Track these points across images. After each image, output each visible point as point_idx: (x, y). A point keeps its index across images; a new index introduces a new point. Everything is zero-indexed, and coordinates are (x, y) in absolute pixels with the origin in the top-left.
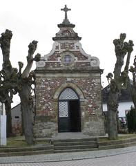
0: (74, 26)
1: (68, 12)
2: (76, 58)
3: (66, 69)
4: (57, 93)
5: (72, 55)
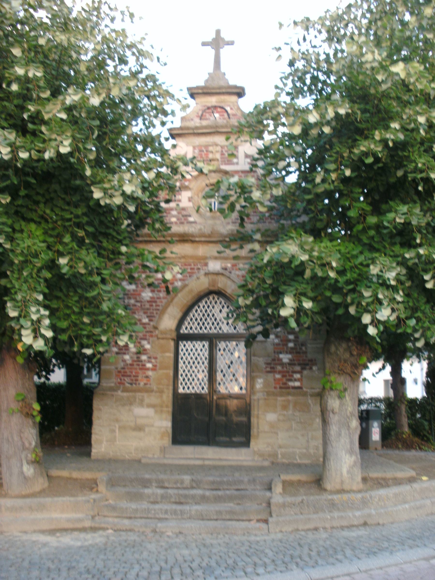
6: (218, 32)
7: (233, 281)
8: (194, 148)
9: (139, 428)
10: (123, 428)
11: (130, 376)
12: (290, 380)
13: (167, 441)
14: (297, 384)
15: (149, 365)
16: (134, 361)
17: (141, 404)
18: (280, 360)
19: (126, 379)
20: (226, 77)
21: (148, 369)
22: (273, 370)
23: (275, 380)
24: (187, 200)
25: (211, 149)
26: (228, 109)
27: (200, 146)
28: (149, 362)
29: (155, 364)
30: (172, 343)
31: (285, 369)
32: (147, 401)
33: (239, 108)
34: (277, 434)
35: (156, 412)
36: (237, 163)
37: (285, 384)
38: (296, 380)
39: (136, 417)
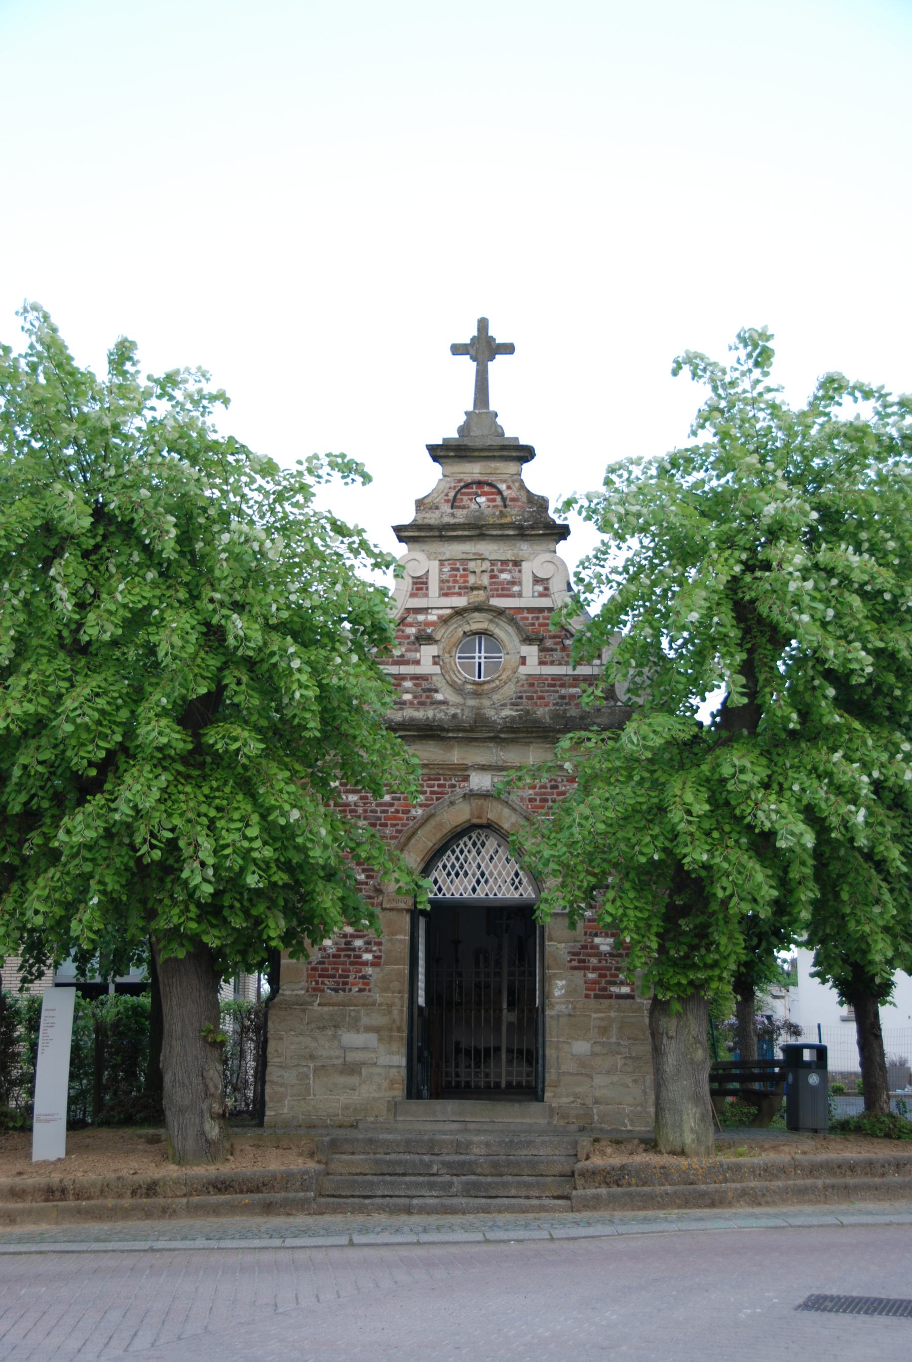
0: (525, 454)
1: (498, 366)
2: (531, 652)
3: (466, 716)
4: (413, 859)
5: (504, 632)
6: (483, 324)
7: (514, 810)
8: (442, 563)
9: (351, 1069)
10: (321, 1070)
11: (333, 976)
12: (614, 983)
13: (399, 1091)
14: (625, 990)
15: (368, 957)
16: (339, 950)
17: (355, 1026)
18: (596, 947)
19: (326, 980)
20: (499, 421)
21: (365, 964)
22: (582, 966)
23: (586, 982)
24: (430, 660)
25: (472, 565)
26: (503, 487)
27: (453, 561)
28: (367, 951)
29: (378, 954)
30: (407, 918)
31: (603, 963)
32: (365, 1021)
33: (522, 486)
34: (592, 1078)
35: (380, 1040)
36: (520, 595)
37: (605, 989)
38: (622, 983)
39: (345, 1049)
